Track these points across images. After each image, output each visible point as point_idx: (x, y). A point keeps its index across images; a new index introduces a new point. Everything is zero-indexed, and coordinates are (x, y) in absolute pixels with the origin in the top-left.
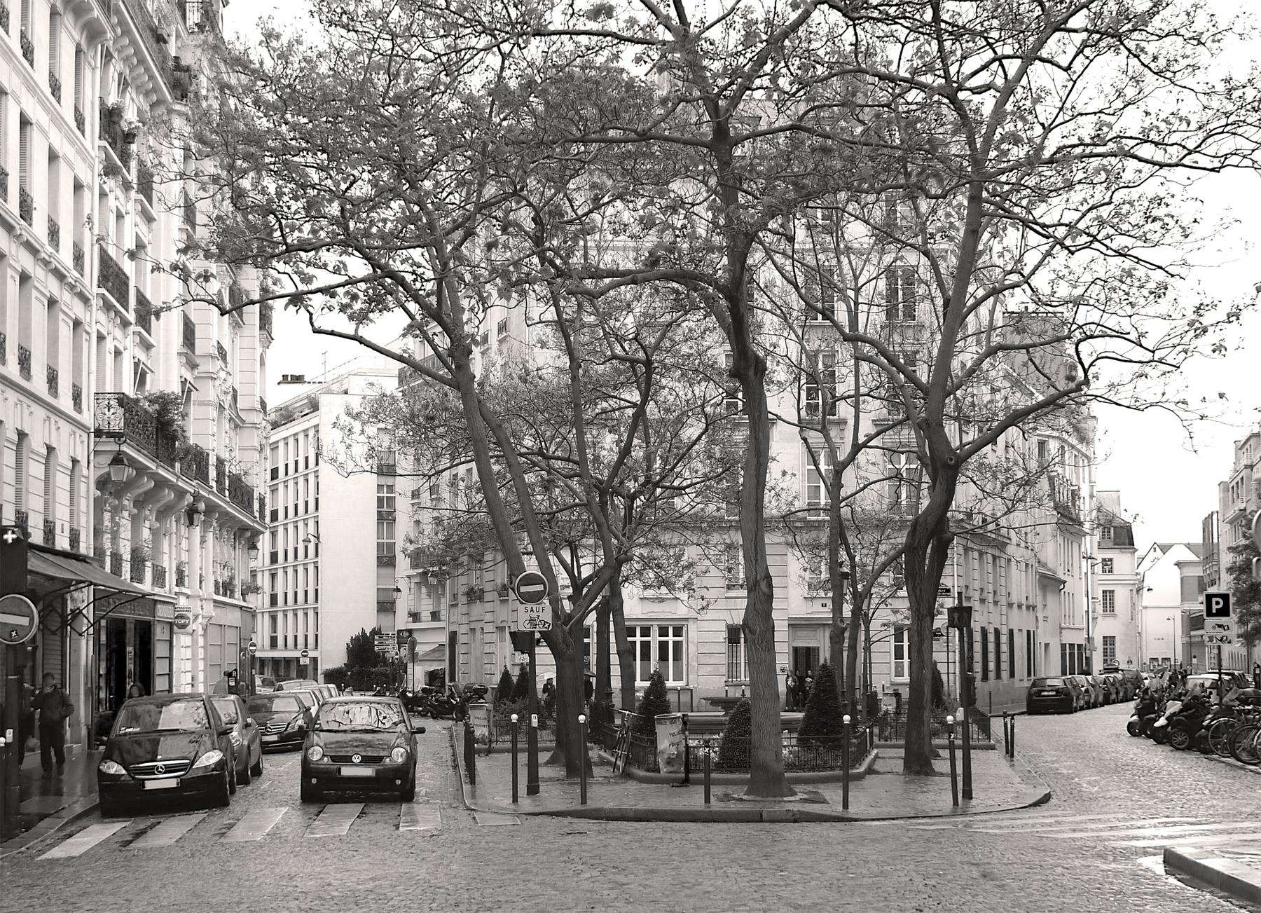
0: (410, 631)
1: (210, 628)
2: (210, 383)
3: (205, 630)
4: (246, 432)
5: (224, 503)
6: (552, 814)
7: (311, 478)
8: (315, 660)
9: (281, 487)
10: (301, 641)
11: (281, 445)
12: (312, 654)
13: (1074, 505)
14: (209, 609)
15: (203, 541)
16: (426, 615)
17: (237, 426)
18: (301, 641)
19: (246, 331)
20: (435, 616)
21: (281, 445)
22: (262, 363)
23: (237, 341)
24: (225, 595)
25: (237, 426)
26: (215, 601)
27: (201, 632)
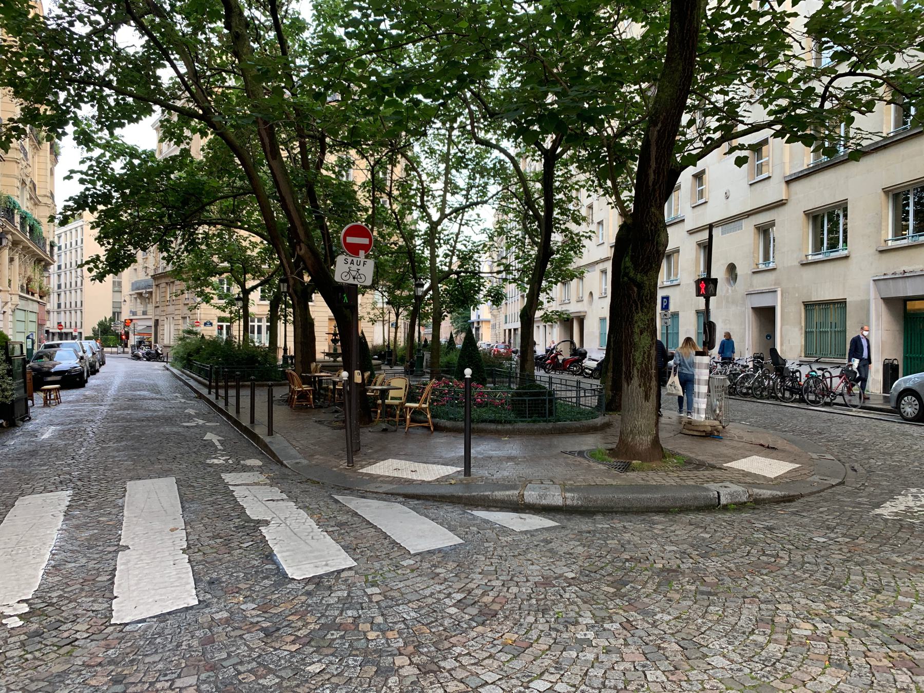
0: (131, 320)
1: (17, 311)
2: (15, 165)
3: (13, 311)
4: (41, 208)
5: (25, 239)
6: (11, 616)
7: (79, 250)
8: (81, 333)
9: (63, 254)
10: (73, 324)
11: (63, 235)
12: (79, 330)
13: (692, 12)
14: (16, 299)
15: (11, 260)
16: (140, 312)
17: (36, 204)
18: (73, 324)
19: (41, 153)
20: (145, 313)
21: (63, 235)
22: (52, 174)
23: (36, 158)
24: (28, 293)
25: (36, 204)
26: (20, 296)
27: (10, 312)
